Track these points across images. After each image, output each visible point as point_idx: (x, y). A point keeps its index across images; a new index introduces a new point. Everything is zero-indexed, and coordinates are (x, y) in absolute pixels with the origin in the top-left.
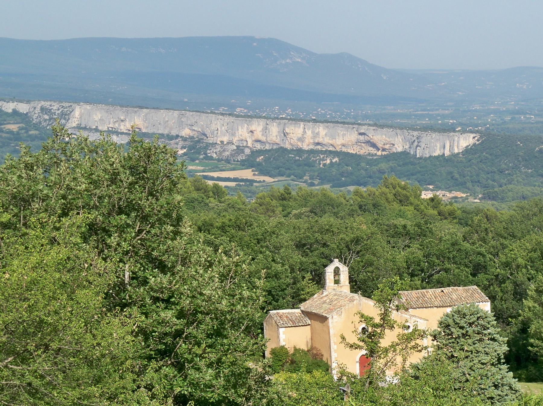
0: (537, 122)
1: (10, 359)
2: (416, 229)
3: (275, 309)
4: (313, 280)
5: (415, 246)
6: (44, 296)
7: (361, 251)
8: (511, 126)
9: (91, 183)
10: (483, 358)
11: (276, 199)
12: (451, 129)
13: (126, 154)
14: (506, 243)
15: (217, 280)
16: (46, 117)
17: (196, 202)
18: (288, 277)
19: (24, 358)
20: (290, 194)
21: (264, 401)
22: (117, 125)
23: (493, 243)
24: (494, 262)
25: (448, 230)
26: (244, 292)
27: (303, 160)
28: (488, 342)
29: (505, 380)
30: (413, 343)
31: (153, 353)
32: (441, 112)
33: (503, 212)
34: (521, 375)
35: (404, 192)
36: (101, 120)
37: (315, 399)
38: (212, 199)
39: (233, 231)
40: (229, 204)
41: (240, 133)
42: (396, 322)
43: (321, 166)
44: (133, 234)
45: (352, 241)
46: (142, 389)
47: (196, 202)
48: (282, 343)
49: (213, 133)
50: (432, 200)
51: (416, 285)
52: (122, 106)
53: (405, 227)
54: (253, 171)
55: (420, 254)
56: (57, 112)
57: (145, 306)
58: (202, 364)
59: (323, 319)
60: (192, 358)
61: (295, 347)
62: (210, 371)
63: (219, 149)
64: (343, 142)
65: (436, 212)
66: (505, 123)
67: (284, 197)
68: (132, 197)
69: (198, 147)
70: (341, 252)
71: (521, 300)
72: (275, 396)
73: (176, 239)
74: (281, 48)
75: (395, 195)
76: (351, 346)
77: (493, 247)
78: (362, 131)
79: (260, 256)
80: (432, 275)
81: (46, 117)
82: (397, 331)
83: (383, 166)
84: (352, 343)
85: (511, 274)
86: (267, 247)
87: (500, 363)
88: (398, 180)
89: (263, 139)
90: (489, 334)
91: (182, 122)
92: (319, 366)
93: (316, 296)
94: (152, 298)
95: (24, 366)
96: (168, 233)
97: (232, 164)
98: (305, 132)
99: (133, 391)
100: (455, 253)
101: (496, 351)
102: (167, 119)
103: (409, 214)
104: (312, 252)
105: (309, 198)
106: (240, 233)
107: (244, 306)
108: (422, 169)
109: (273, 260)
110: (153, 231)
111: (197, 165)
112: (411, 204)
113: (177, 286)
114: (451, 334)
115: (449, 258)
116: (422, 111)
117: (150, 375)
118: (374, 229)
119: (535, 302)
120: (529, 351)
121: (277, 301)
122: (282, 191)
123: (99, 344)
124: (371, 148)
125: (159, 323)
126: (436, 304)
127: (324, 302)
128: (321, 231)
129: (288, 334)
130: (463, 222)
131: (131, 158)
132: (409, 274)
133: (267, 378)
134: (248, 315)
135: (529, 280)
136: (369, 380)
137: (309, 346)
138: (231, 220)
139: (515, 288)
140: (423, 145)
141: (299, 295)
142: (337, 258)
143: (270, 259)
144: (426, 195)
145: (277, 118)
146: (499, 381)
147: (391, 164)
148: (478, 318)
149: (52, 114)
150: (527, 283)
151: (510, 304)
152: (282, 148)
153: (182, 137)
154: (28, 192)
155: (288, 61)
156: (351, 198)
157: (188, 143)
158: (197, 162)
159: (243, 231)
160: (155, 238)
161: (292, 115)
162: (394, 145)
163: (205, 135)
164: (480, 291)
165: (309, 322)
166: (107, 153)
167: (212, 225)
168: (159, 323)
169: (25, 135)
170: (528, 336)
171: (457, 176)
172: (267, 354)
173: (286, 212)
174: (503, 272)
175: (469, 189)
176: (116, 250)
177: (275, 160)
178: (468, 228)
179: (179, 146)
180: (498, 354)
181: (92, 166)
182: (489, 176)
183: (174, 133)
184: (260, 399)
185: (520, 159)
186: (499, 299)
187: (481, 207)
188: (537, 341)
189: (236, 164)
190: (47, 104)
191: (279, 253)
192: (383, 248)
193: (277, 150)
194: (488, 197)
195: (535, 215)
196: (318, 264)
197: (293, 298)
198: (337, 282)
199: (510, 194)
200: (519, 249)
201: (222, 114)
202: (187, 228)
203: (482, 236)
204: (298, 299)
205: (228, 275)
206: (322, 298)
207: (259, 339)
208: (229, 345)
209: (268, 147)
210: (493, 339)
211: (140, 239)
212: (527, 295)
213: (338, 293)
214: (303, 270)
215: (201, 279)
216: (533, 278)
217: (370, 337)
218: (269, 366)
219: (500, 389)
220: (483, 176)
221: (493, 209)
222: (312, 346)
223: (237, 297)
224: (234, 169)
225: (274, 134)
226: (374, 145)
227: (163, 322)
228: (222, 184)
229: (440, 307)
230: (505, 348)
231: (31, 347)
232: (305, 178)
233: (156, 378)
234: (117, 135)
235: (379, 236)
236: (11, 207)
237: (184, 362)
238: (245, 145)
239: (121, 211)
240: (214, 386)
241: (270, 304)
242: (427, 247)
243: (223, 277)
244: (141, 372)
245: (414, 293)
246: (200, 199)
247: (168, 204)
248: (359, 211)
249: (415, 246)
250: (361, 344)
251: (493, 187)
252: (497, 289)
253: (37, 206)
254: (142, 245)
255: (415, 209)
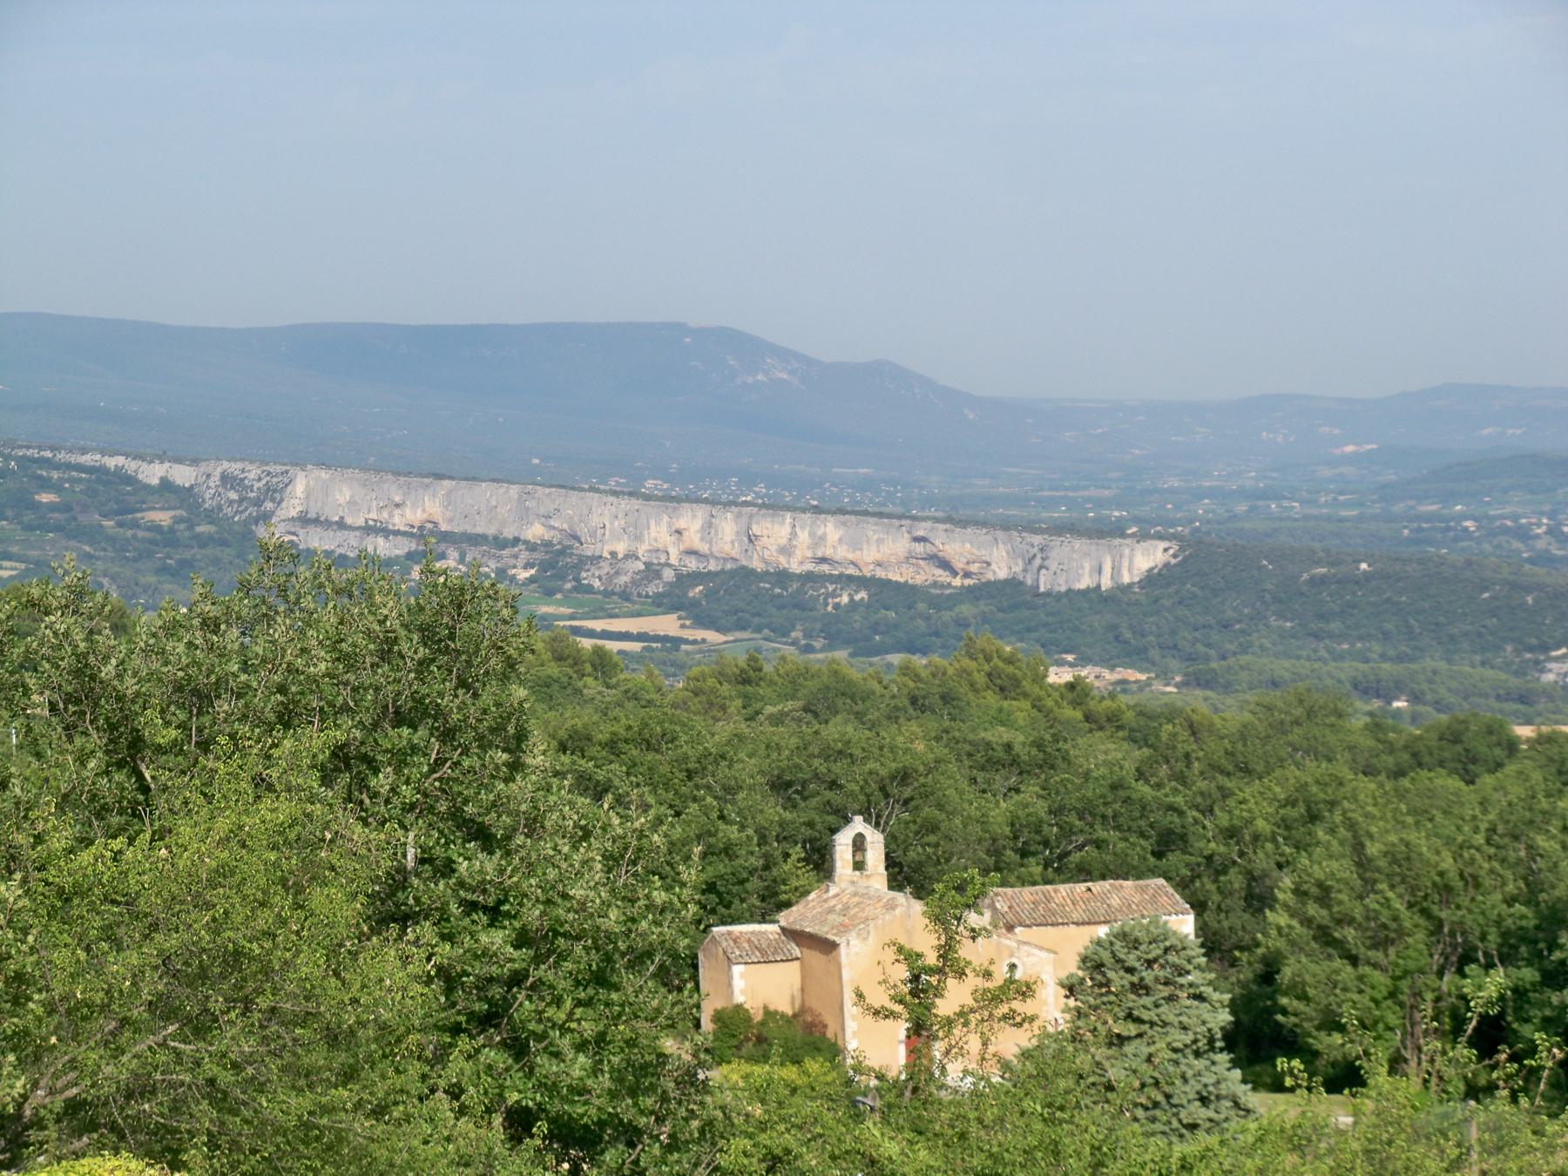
0: (1306, 518)
1: (171, 1029)
2: (1034, 751)
3: (724, 923)
4: (806, 860)
5: (1031, 789)
6: (244, 898)
7: (912, 799)
8: (1247, 525)
9: (338, 659)
10: (1177, 1037)
11: (730, 682)
12: (1115, 531)
13: (412, 600)
14: (1229, 785)
15: (599, 866)
16: (233, 496)
17: (556, 687)
18: (752, 853)
19: (200, 1027)
20: (760, 670)
21: (695, 1124)
22: (385, 515)
23: (1202, 784)
24: (1204, 827)
25: (1104, 755)
26: (655, 893)
27: (790, 595)
28: (1189, 1002)
29: (1223, 1086)
30: (1004, 1009)
31: (462, 1019)
32: (1092, 492)
33: (1227, 715)
34: (1259, 1075)
35: (1010, 669)
36: (352, 503)
37: (798, 1121)
38: (589, 680)
39: (635, 752)
40: (626, 692)
41: (653, 535)
42: (969, 963)
43: (830, 608)
44: (425, 769)
45: (893, 778)
46: (440, 1094)
47: (556, 687)
48: (739, 998)
49: (593, 534)
50: (1071, 686)
51: (1031, 875)
52: (397, 473)
53: (1008, 747)
54: (680, 618)
55: (1041, 808)
56: (257, 485)
57: (447, 920)
58: (565, 1043)
59: (828, 947)
60: (545, 1032)
61: (765, 1008)
62: (582, 1058)
63: (606, 568)
64: (879, 556)
65: (1079, 715)
66: (1234, 518)
67: (747, 678)
68: (425, 690)
69: (559, 565)
70: (869, 802)
71: (1261, 910)
72: (719, 1114)
73: (514, 780)
74: (748, 348)
75: (989, 675)
76: (876, 1013)
77: (1202, 794)
78: (921, 533)
79: (694, 808)
80: (1066, 854)
81: (233, 496)
82: (973, 981)
83: (966, 610)
84: (877, 1005)
85: (1241, 854)
86: (708, 787)
87: (1212, 1049)
88: (999, 642)
89: (704, 548)
90: (1191, 985)
91: (528, 509)
92: (818, 1049)
93: (812, 896)
94: (462, 902)
95: (201, 1045)
96: (497, 768)
97: (635, 603)
98: (794, 534)
99: (421, 1100)
100: (1117, 806)
101: (1204, 1023)
102: (494, 503)
103: (1021, 718)
104: (805, 799)
105: (801, 680)
106: (649, 758)
107: (656, 923)
108: (1050, 619)
109: (722, 817)
110: (466, 763)
111: (559, 603)
112: (1026, 695)
113: (515, 879)
114: (1107, 984)
115: (1104, 817)
116: (1051, 489)
117: (457, 1067)
118: (941, 751)
119: (1292, 916)
120: (1277, 1023)
121: (728, 906)
122: (743, 664)
123: (354, 1001)
124: (939, 572)
125: (476, 957)
126: (1075, 916)
127: (831, 910)
128: (828, 754)
129: (751, 977)
130: (1137, 738)
131: (422, 609)
132: (1016, 851)
133: (701, 1076)
134: (663, 942)
135: (1280, 866)
136: (911, 1085)
137: (797, 1006)
138: (629, 728)
139: (1249, 885)
140: (1053, 566)
141: (776, 894)
142: (860, 813)
143: (715, 815)
144: (1059, 676)
145: (734, 503)
146: (1211, 1088)
147: (983, 606)
148: (1166, 950)
149: (245, 488)
150: (1275, 873)
151: (1237, 919)
152: (743, 568)
153: (526, 542)
154: (208, 676)
155: (760, 377)
156: (893, 681)
157: (539, 556)
158: (559, 596)
159: (657, 751)
160: (470, 777)
161: (767, 495)
162: (989, 564)
163: (576, 538)
164: (1171, 890)
165: (797, 952)
166: (371, 596)
167: (589, 739)
168: (476, 957)
169: (187, 534)
170: (1275, 992)
171: (1128, 635)
172: (707, 1025)
173: (750, 711)
174: (1222, 849)
175: (1154, 664)
176: (387, 802)
177: (730, 594)
178: (1146, 751)
179: (520, 563)
180: (1209, 1030)
181: (341, 623)
182: (1197, 634)
183: (509, 533)
184: (686, 1119)
185: (1268, 597)
186: (1214, 907)
187: (1180, 704)
188: (1295, 1003)
189: (643, 604)
190: (234, 468)
191: (733, 802)
192: (961, 793)
193: (732, 574)
194: (1197, 680)
195: (1297, 723)
196: (819, 827)
197: (763, 900)
198: (859, 866)
199: (1244, 675)
200: (1259, 799)
201: (615, 493)
202: (538, 756)
203: (1177, 769)
204: (772, 903)
205: (622, 857)
206: (825, 901)
207: (686, 993)
208: (622, 1005)
209: (713, 566)
210: (1199, 997)
211: (440, 779)
212: (1276, 900)
213: (862, 891)
214: (785, 838)
215: (564, 865)
216: (1288, 862)
217: (919, 991)
218: (707, 1051)
219: (1212, 1106)
220: (1186, 634)
221: (1204, 709)
222: (803, 1006)
223: (642, 903)
224: (639, 615)
225: (728, 538)
226: (945, 565)
227: (484, 954)
228: (613, 646)
229: (1083, 923)
230: (1225, 1017)
231: (217, 1004)
232: (793, 634)
233: (468, 1072)
234: (386, 537)
235: (952, 767)
236: (173, 708)
237: (527, 1039)
238: (663, 561)
239: (400, 720)
240: (589, 1092)
241: (713, 911)
242: (1057, 793)
243: (612, 861)
244: (441, 1057)
245: (1027, 893)
246: (565, 680)
247: (498, 705)
248: (911, 710)
249: (1031, 789)
250: (898, 1008)
251: (1207, 659)
252: (1210, 887)
253: (226, 707)
254: (444, 791)
255: (1034, 706)
